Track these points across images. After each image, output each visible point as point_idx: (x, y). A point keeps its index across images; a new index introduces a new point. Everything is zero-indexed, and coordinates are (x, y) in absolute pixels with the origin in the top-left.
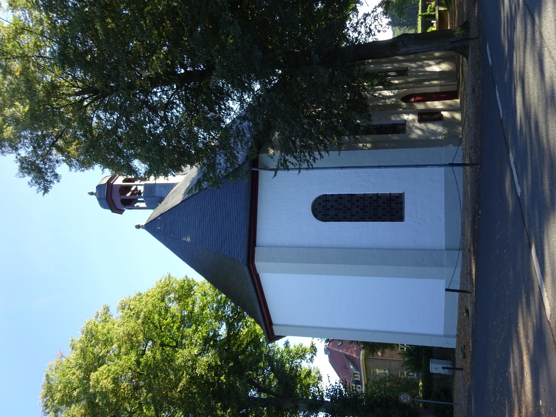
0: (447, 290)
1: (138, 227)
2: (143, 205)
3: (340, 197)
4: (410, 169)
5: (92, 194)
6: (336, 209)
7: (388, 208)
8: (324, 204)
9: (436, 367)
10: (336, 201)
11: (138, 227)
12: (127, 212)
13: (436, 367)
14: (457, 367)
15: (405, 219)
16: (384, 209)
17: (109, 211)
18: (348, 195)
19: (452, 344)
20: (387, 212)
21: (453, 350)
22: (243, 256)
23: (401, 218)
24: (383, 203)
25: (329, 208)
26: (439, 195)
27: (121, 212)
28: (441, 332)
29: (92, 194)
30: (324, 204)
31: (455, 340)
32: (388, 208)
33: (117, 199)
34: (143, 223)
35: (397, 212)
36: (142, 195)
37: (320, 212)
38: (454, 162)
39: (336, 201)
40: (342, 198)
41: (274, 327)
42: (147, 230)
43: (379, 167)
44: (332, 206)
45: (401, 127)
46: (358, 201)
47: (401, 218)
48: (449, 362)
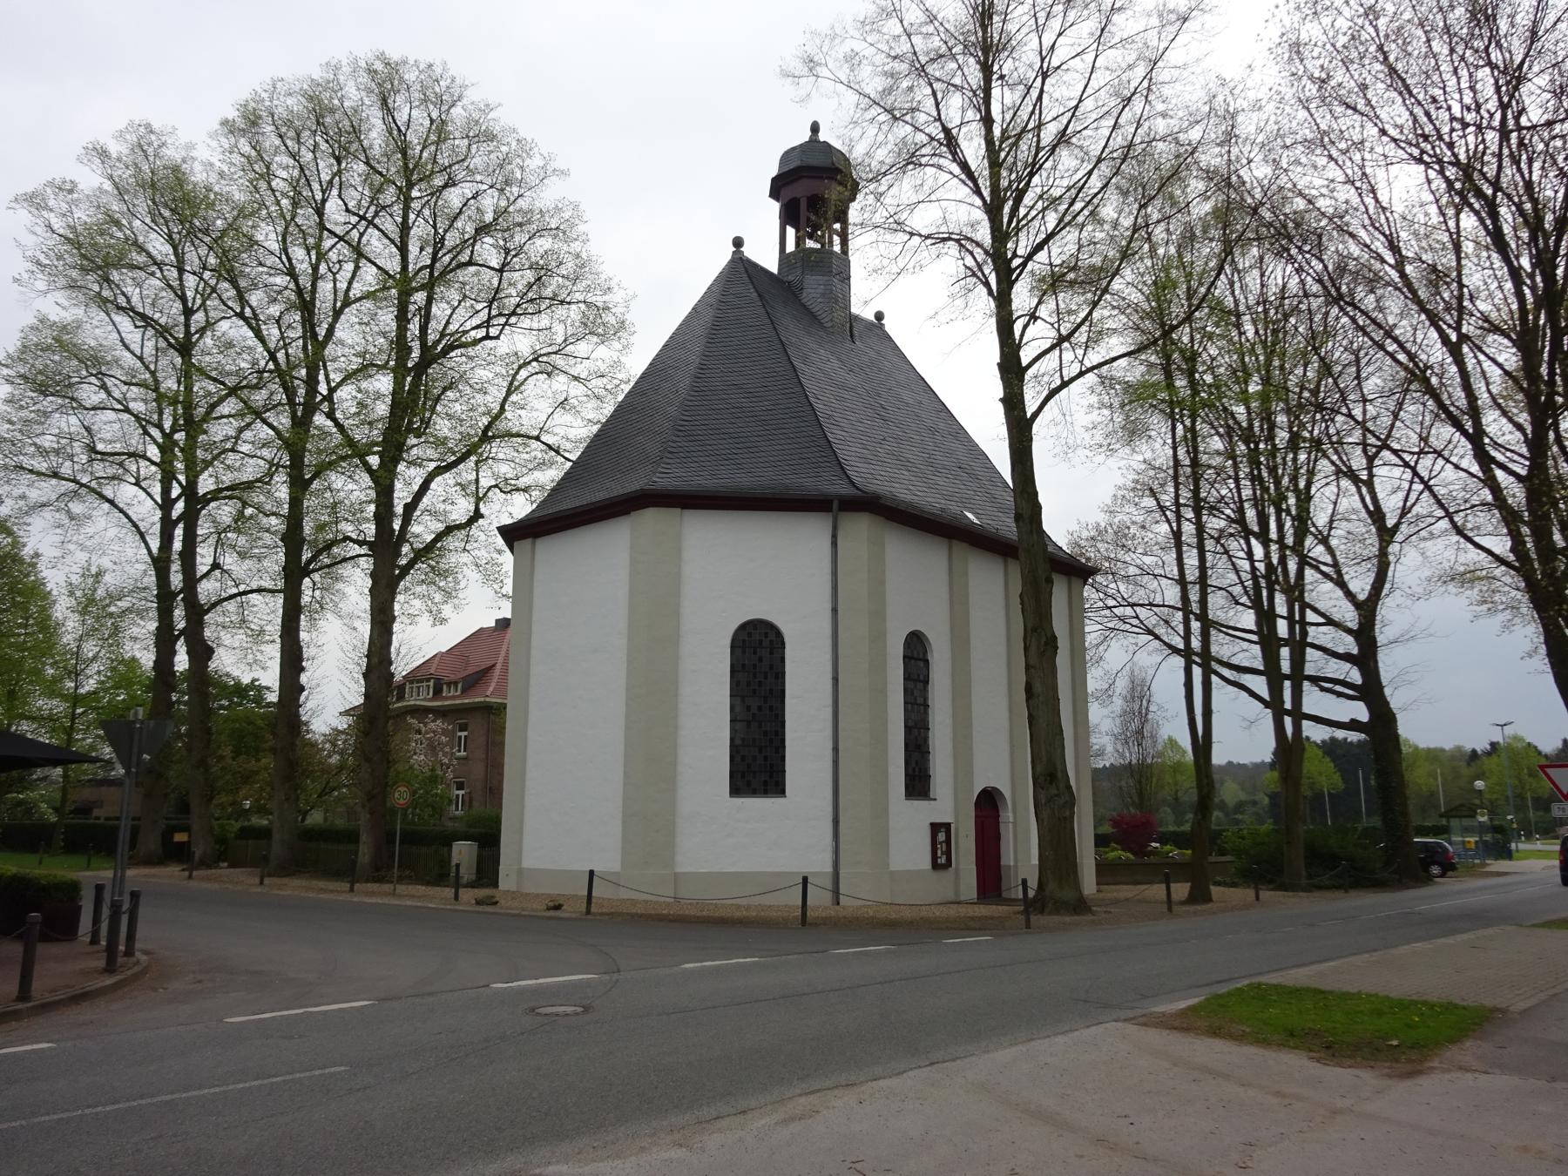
0: (592, 873)
1: (738, 243)
2: (791, 246)
3: (780, 676)
4: (830, 809)
5: (815, 128)
6: (755, 666)
7: (757, 766)
8: (766, 643)
9: (463, 853)
10: (771, 667)
11: (738, 243)
12: (775, 206)
13: (463, 853)
14: (461, 891)
15: (740, 801)
16: (755, 758)
17: (774, 171)
18: (783, 691)
19: (506, 881)
20: (749, 766)
21: (495, 884)
22: (664, 481)
23: (736, 791)
24: (766, 758)
25: (758, 655)
26: (529, 842)
27: (775, 193)
28: (527, 863)
29: (815, 128)
30: (766, 643)
31: (514, 888)
32: (757, 766)
33: (801, 190)
34: (748, 251)
35: (749, 784)
36: (810, 244)
37: (750, 635)
38: (830, 887)
39: (771, 667)
40: (777, 677)
41: (529, 541)
42: (732, 261)
43: (836, 749)
44: (760, 660)
45: (1106, 784)
46: (771, 708)
47: (736, 791)
48: (473, 877)
